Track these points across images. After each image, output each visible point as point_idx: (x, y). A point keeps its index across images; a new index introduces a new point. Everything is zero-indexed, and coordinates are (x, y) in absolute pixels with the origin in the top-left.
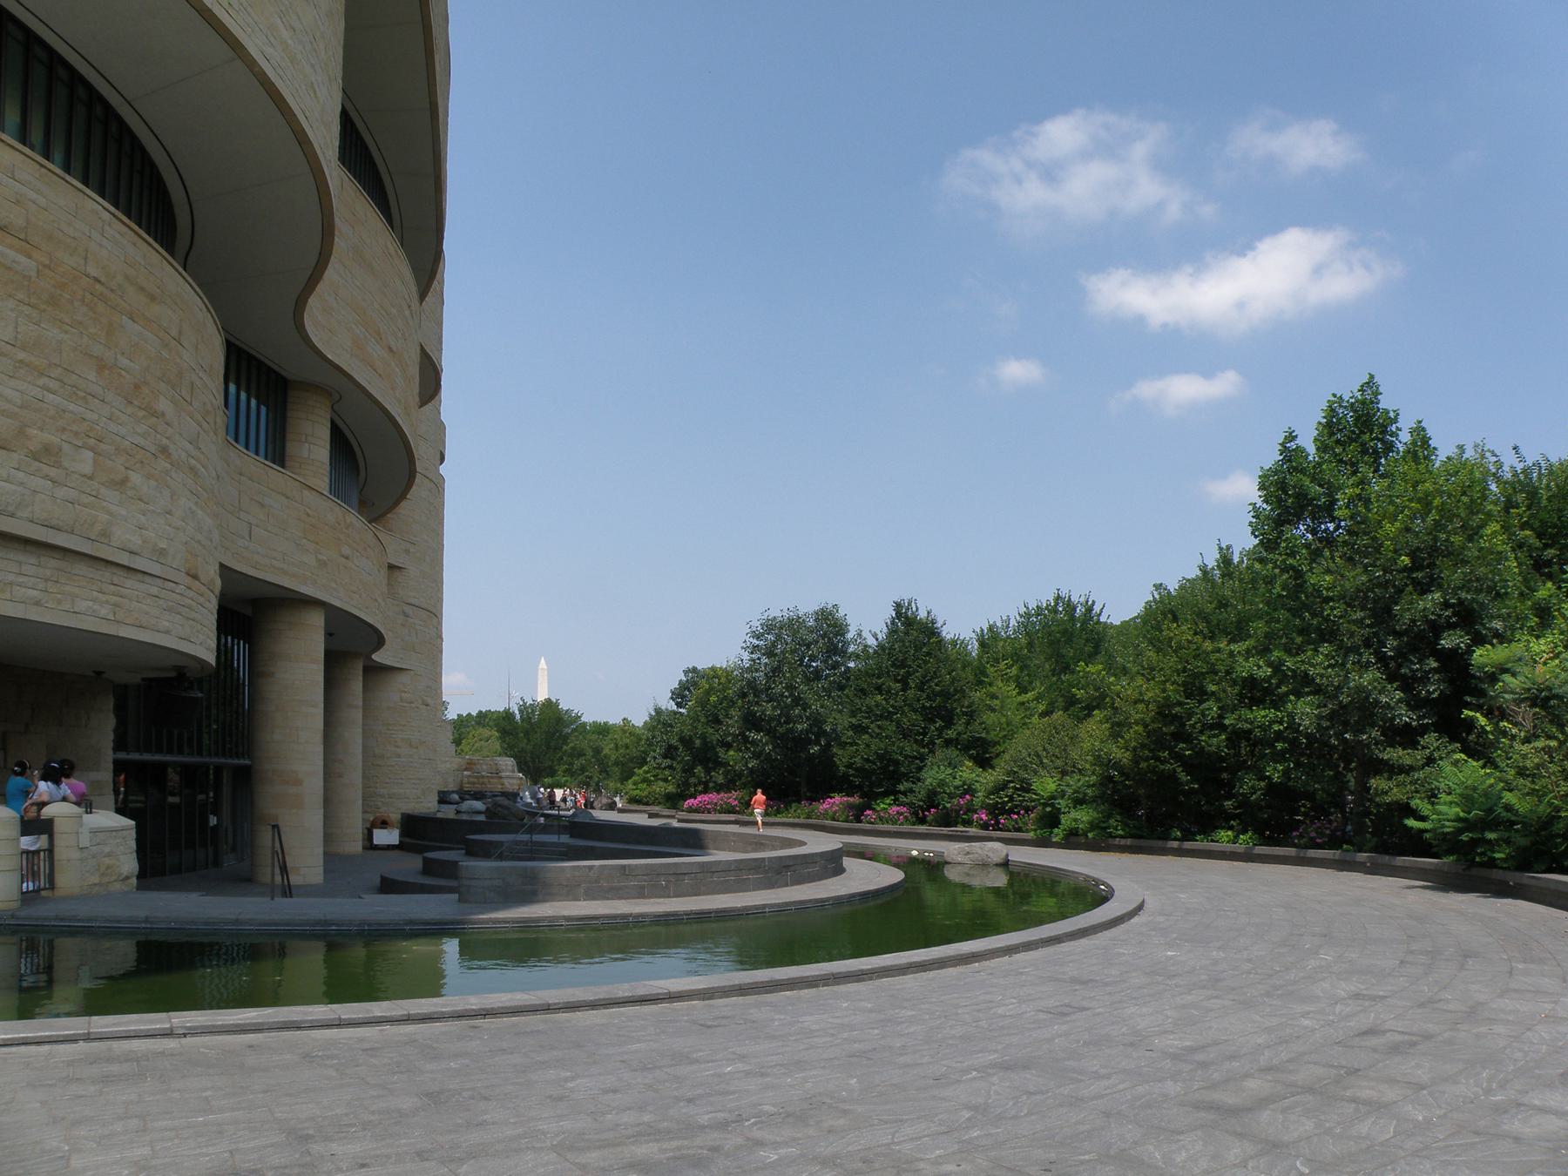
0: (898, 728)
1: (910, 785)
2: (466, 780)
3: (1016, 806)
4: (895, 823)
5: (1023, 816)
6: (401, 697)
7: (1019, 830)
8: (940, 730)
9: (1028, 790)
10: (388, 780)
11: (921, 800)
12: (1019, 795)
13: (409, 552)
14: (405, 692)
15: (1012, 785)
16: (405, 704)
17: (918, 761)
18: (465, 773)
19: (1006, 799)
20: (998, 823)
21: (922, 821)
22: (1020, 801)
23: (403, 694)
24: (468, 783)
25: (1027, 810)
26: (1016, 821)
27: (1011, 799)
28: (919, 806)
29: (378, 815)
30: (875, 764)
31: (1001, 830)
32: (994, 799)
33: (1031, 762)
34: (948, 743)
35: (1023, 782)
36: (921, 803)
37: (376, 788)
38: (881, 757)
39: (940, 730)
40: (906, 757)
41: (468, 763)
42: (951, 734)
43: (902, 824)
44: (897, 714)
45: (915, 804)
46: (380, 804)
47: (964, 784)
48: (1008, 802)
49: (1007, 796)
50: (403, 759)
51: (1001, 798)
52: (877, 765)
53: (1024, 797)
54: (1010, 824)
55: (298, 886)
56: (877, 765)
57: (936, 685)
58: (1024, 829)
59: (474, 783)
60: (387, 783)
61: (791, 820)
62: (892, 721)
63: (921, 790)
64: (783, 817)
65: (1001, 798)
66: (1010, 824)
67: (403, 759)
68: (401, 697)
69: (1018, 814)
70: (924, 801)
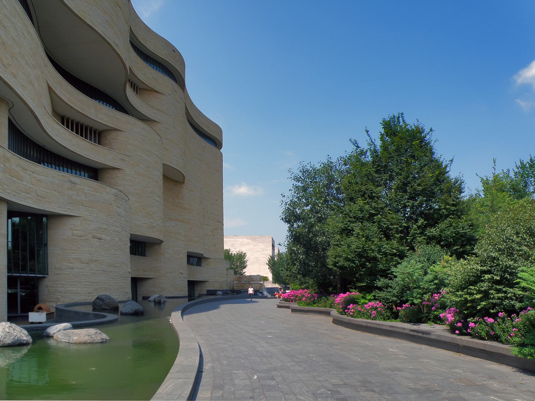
0: (379, 228)
1: (387, 281)
2: (235, 285)
3: (494, 306)
4: (369, 317)
5: (503, 319)
6: (72, 233)
7: (496, 338)
8: (423, 228)
9: (512, 285)
10: (64, 283)
11: (394, 295)
12: (499, 291)
13: (125, 160)
14: (76, 230)
15: (487, 276)
16: (75, 237)
17: (397, 258)
18: (235, 282)
19: (478, 296)
20: (466, 325)
21: (396, 316)
22: (499, 298)
23: (74, 232)
24: (236, 286)
25: (511, 311)
26: (492, 327)
27: (486, 295)
28: (393, 301)
29: (59, 303)
30: (353, 262)
31: (469, 334)
32: (461, 296)
33: (519, 244)
34: (430, 240)
35: (505, 272)
36: (395, 299)
37: (57, 287)
38: (360, 256)
39: (423, 228)
40: (385, 254)
41: (238, 278)
42: (433, 231)
43: (375, 318)
44: (377, 215)
45: (389, 299)
46: (59, 297)
47: (436, 278)
48: (481, 300)
49: (479, 292)
50: (76, 270)
51: (471, 294)
52: (355, 263)
53: (505, 292)
54: (481, 329)
55: (332, 315)
56: (355, 263)
57: (419, 185)
58: (503, 338)
59: (239, 287)
60: (63, 284)
61: (322, 309)
62: (374, 222)
63: (397, 284)
64: (316, 306)
65: (471, 294)
66: (481, 329)
67: (76, 270)
68: (72, 233)
69: (495, 316)
70: (397, 296)
